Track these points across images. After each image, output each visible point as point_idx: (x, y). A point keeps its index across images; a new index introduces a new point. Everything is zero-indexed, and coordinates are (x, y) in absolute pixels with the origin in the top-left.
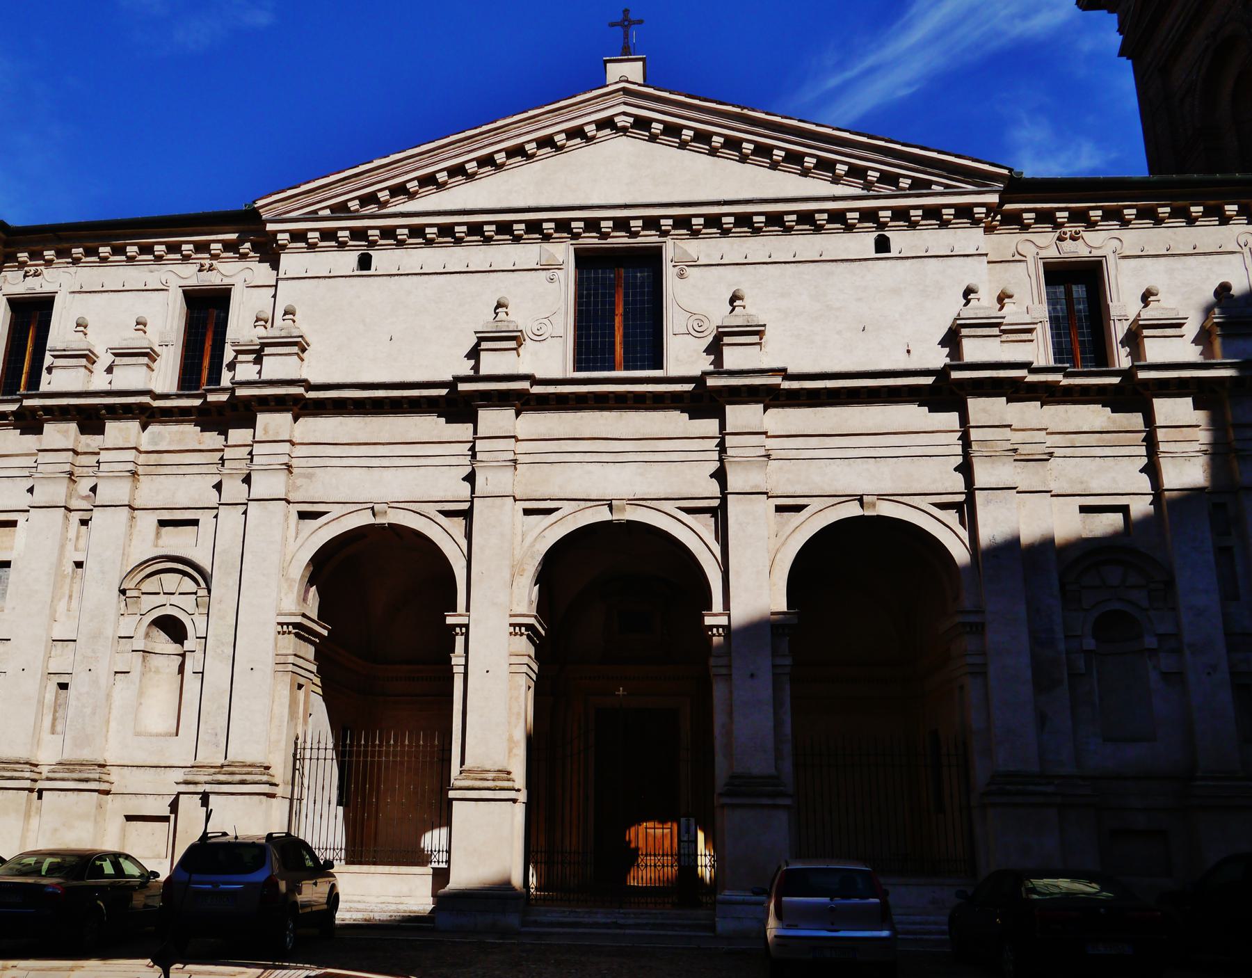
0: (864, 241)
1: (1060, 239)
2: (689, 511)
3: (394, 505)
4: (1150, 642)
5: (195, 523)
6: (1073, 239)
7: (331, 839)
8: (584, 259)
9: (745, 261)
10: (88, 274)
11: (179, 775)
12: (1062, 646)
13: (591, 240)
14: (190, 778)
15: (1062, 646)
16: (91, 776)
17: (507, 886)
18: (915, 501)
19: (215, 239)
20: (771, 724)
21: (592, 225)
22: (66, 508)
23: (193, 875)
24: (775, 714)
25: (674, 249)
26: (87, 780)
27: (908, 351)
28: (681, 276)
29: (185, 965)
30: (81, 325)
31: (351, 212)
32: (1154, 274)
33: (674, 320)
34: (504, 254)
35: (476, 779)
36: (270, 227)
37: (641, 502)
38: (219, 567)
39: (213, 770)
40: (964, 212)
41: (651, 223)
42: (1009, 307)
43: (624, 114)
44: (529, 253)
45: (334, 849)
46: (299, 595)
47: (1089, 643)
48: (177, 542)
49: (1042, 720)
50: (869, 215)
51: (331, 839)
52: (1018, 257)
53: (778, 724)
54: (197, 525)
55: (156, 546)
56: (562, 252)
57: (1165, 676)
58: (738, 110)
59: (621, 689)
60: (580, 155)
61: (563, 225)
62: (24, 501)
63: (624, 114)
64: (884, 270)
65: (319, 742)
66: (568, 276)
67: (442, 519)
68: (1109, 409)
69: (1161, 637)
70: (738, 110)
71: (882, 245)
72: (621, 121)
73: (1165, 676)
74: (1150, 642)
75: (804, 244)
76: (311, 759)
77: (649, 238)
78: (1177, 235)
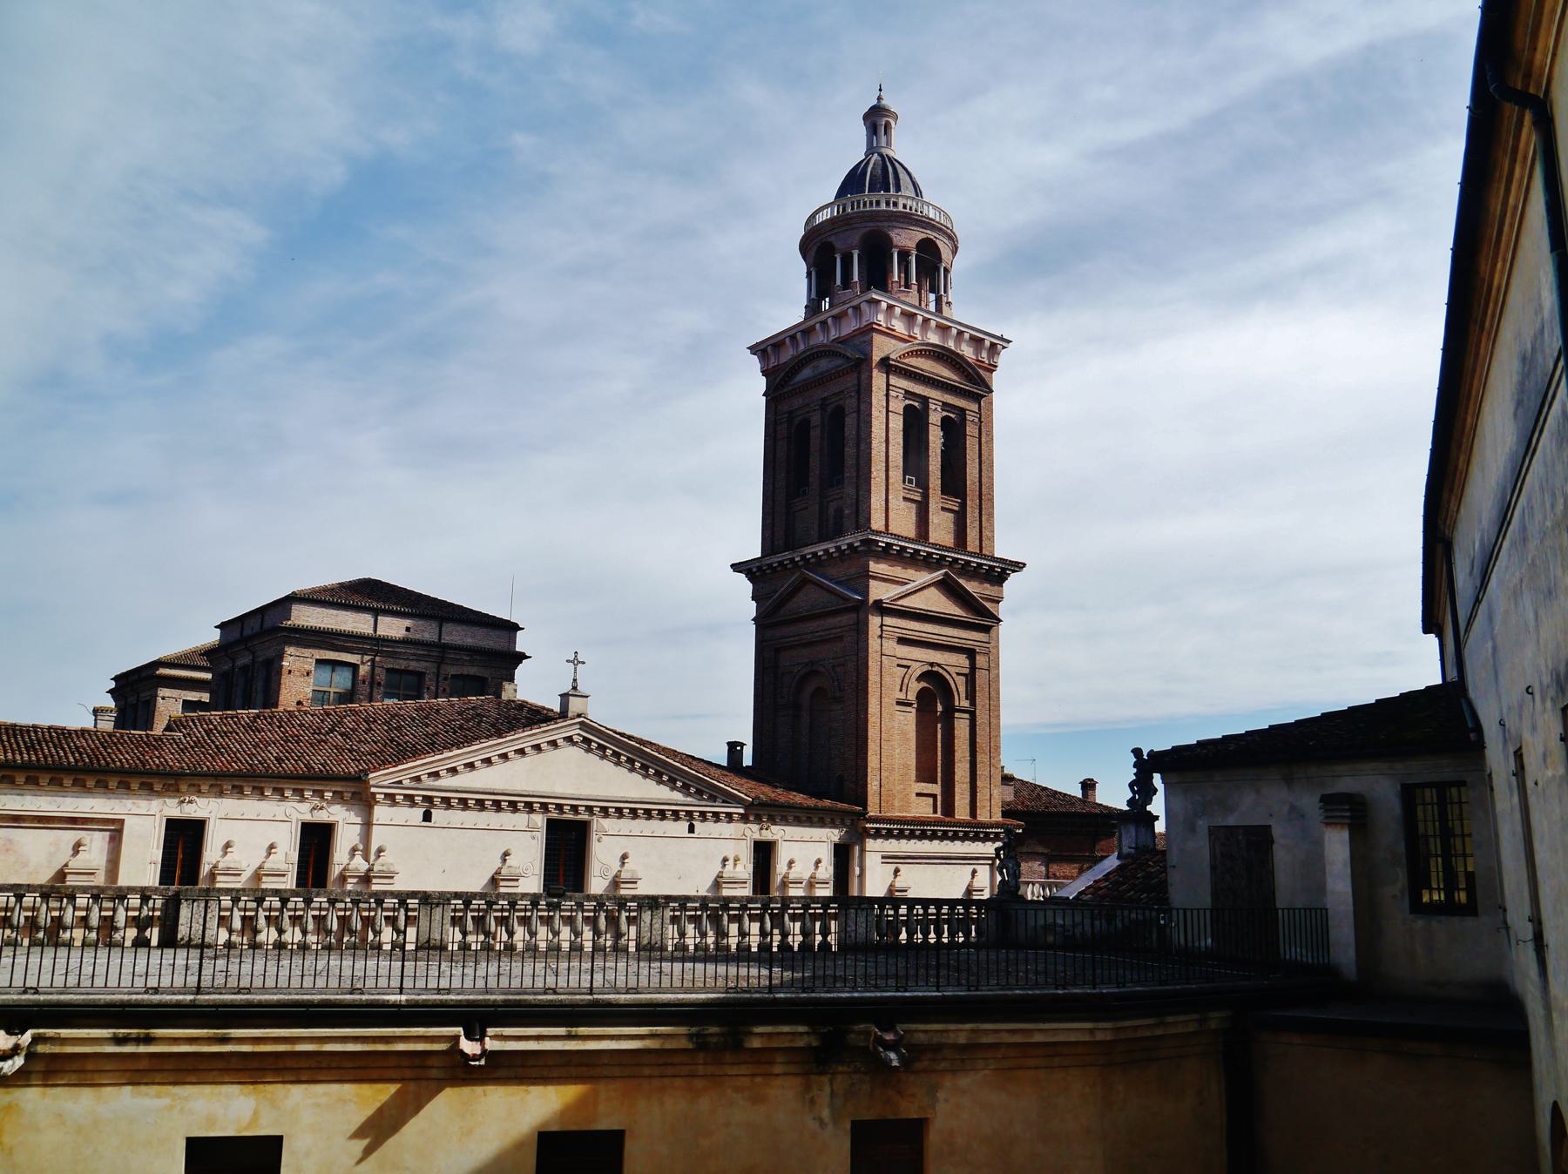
0: (683, 826)
1: (761, 829)
6: (767, 829)
8: (551, 824)
13: (554, 815)
17: (1448, 801)
19: (958, 755)
21: (559, 807)
23: (685, 964)
25: (600, 824)
28: (599, 841)
29: (1437, 804)
31: (656, 770)
34: (506, 819)
36: (373, 790)
40: (729, 816)
41: (589, 809)
43: (579, 735)
44: (521, 819)
50: (689, 814)
52: (744, 837)
56: (539, 820)
58: (638, 745)
59: (876, 906)
61: (544, 806)
63: (579, 735)
66: (541, 836)
68: (1156, 823)
70: (638, 745)
72: (576, 739)
75: (656, 826)
77: (584, 817)
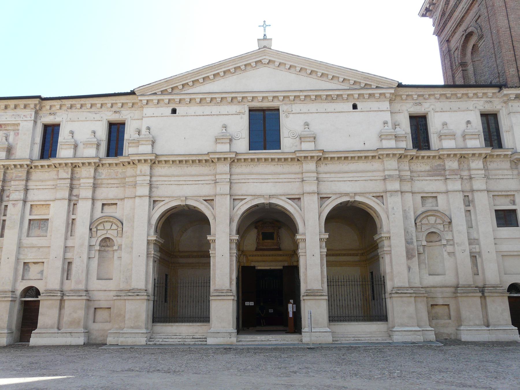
2: (289, 199)
3: (194, 197)
4: (444, 242)
5: (116, 204)
7: (336, 313)
9: (308, 112)
10: (73, 114)
11: (114, 293)
12: (415, 244)
14: (118, 294)
15: (415, 244)
16: (82, 294)
18: (367, 195)
20: (320, 272)
22: (413, 193)
24: (321, 268)
26: (81, 296)
27: (364, 144)
30: (72, 133)
32: (446, 117)
33: (284, 132)
34: (313, 107)
35: (220, 293)
37: (177, 198)
38: (126, 220)
39: (127, 292)
42: (398, 129)
44: (234, 108)
45: (343, 317)
46: (154, 230)
47: (424, 243)
48: (429, 205)
49: (409, 268)
51: (336, 313)
53: (322, 272)
54: (117, 205)
55: (102, 213)
57: (449, 253)
60: (251, 73)
62: (443, 188)
64: (355, 114)
65: (344, 279)
67: (374, 199)
69: (448, 241)
71: (355, 107)
73: (449, 253)
74: (444, 242)
76: (376, 285)
78: (455, 104)
